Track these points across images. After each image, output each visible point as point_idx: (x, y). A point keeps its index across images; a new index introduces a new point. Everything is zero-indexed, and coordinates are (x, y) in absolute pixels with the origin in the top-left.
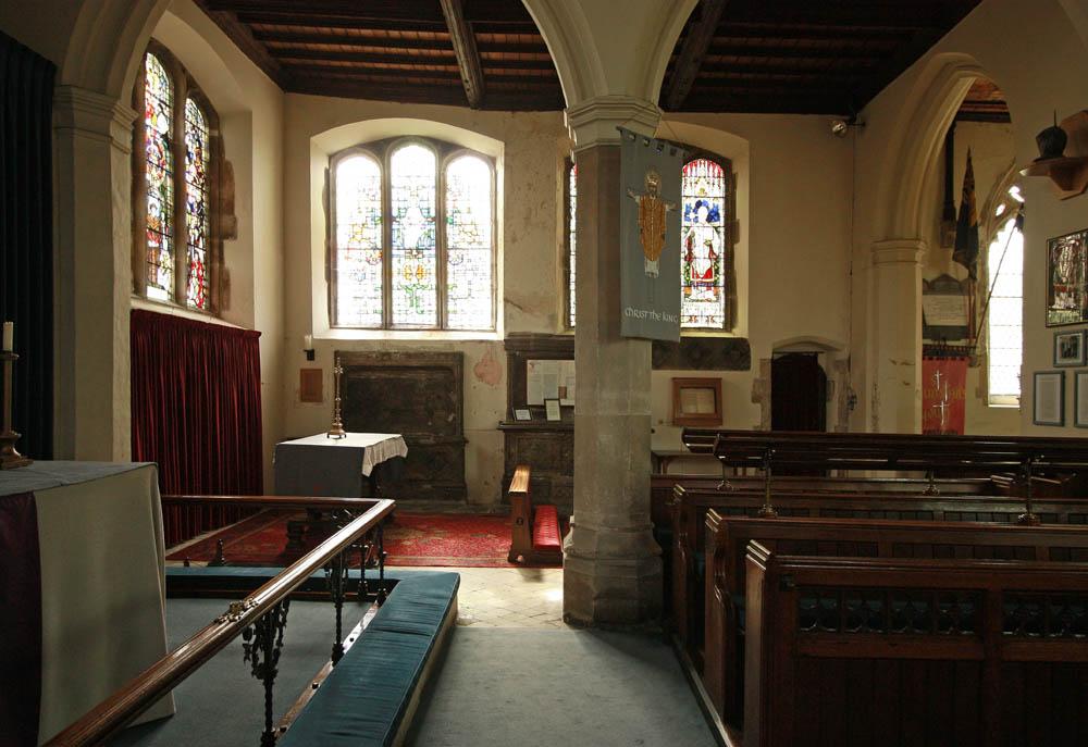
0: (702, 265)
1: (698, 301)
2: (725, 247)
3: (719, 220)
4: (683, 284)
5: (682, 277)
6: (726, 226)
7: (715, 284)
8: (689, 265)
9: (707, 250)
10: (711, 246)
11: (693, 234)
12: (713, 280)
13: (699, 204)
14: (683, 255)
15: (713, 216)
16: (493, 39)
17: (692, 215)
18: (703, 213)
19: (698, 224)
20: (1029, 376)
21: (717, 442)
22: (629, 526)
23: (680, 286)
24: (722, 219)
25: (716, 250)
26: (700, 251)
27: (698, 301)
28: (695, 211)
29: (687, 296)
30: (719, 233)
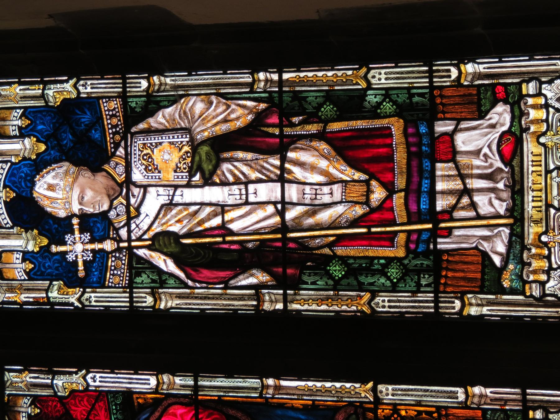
0: (316, 187)
1: (516, 213)
2: (225, 65)
3: (92, 103)
4: (425, 302)
5: (384, 303)
6: (119, 65)
7: (420, 110)
8: (321, 264)
9: (239, 163)
10: (224, 144)
11: (163, 241)
12: (396, 127)
13: (26, 212)
14: (273, 302)
15: (76, 138)
16: (416, 167)
17: (78, 248)
18: (61, 191)
19: (118, 216)
20: (392, 63)
21: (401, 238)
22: (71, 180)
23: (436, 319)
24: (88, 88)
25: (240, 115)
26: (247, 203)
27: (516, 213)
28: (55, 228)
29: (488, 278)
30: (153, 103)
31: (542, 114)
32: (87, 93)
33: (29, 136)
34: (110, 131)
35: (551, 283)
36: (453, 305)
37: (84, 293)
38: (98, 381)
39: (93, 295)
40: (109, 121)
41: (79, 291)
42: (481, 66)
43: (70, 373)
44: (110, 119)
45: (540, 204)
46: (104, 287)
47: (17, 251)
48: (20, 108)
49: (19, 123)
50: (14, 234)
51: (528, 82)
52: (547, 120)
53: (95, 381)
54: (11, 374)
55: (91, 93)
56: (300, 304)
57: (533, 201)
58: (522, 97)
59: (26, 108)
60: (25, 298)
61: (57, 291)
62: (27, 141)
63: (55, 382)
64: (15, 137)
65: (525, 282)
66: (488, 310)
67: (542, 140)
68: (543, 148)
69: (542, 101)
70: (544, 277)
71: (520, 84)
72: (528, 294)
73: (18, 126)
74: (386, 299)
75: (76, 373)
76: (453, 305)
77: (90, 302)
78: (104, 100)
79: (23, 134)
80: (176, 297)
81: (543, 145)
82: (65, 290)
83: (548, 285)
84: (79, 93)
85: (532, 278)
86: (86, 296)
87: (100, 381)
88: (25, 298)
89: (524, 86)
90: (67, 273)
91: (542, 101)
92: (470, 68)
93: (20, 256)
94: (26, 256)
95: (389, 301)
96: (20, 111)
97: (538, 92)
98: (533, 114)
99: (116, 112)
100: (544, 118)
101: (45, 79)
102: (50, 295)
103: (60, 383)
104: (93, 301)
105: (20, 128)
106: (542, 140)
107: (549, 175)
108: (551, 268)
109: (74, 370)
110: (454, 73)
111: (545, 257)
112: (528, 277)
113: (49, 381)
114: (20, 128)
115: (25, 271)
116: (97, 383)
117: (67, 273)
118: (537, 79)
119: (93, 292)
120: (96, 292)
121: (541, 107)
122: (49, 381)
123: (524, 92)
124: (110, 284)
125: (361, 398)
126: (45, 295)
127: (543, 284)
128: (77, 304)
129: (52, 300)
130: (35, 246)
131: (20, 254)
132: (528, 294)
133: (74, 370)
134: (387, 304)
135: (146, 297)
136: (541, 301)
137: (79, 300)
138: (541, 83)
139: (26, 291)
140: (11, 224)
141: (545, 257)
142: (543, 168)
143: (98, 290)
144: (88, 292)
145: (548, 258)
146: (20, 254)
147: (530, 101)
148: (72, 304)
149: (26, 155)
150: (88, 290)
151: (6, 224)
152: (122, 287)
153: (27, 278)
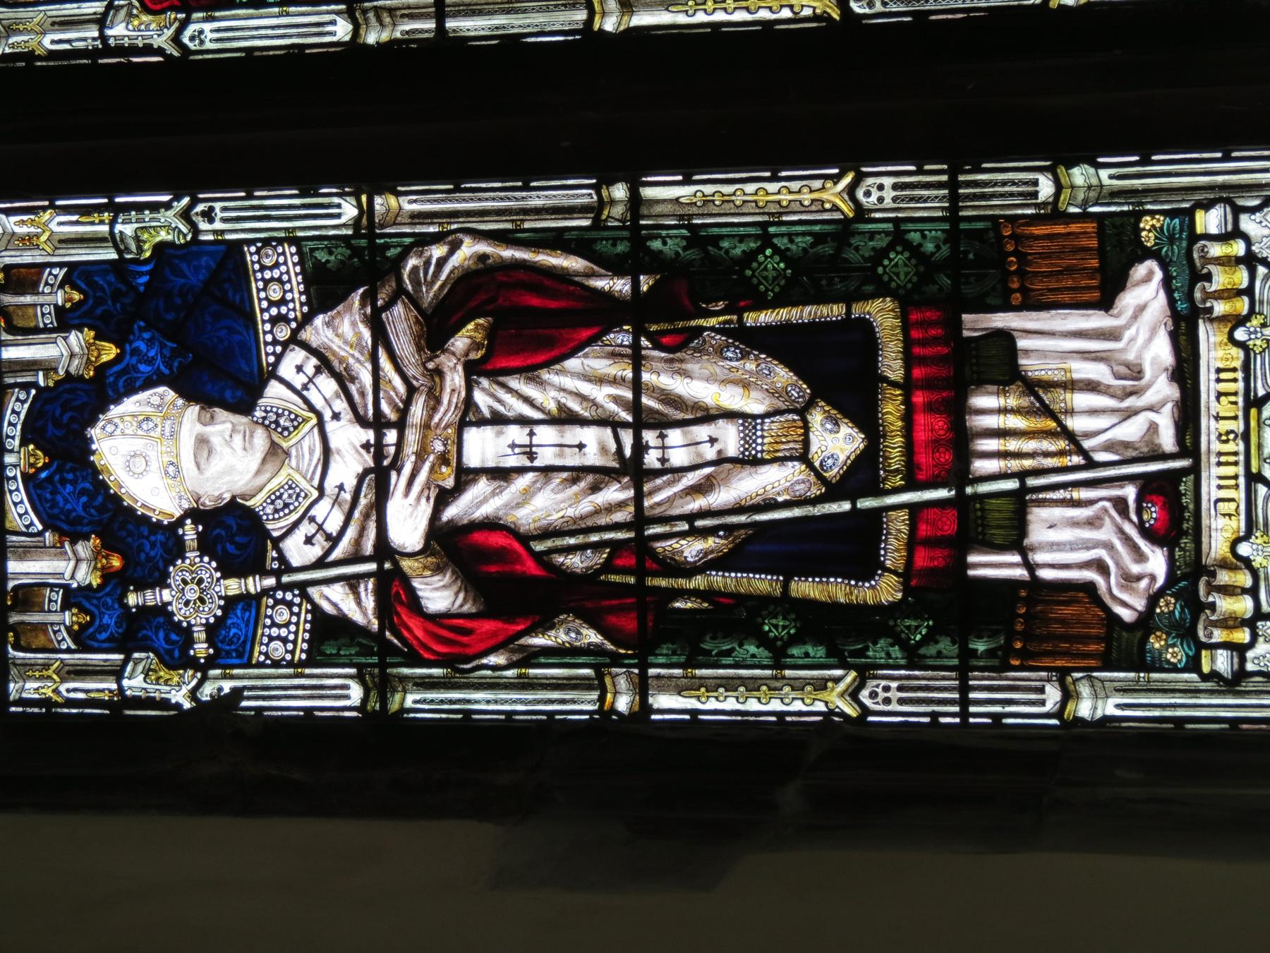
28: (140, 546)
31: (1241, 277)
32: (215, 232)
33: (79, 328)
34: (266, 316)
35: (1261, 648)
36: (1043, 697)
37: (184, 24)
38: (217, 219)
39: (207, 27)
40: (263, 295)
41: (194, 676)
42: (1104, 174)
43: (155, 207)
44: (265, 289)
45: (1230, 471)
46: (249, 665)
47: (52, 586)
48: (60, 265)
49: (60, 298)
50: (45, 547)
51: (1207, 206)
52: (1249, 291)
53: (211, 221)
54: (13, 219)
55: (222, 232)
56: (698, 698)
57: (1219, 464)
58: (1194, 238)
59: (72, 266)
60: (53, 42)
61: (124, 24)
62: (74, 338)
63: (118, 228)
64: (46, 330)
65: (1200, 646)
66: (1118, 706)
67: (1240, 334)
68: (1240, 354)
69: (1239, 248)
70: (1243, 636)
71: (1190, 213)
72: (1206, 669)
73: (56, 306)
74: (894, 685)
75: (167, 206)
76: (1043, 697)
77: (202, 42)
78: (253, 249)
79: (66, 320)
80: (416, 684)
81: (1242, 345)
82: (162, 673)
83: (1250, 654)
84: (195, 230)
85: (1219, 636)
86: (191, 29)
87: (224, 220)
88: (53, 42)
89: (1199, 215)
90: (161, 637)
91: (1239, 248)
92: (1080, 175)
93: (58, 597)
94: (73, 597)
95: (895, 187)
96: (60, 273)
97: (1230, 228)
98: (1221, 279)
99: (282, 274)
100: (1245, 284)
101: (118, 200)
102: (109, 32)
103: (128, 230)
104: (207, 40)
105: (59, 310)
106: (1240, 334)
107: (1253, 411)
108: (1259, 615)
109: (166, 198)
110: (1046, 188)
111: (1244, 591)
112: (1210, 636)
113: (105, 228)
114: (59, 310)
115: (69, 630)
116: (218, 225)
117: (161, 637)
118: (1229, 201)
119: (225, 677)
120: (214, 19)
121: (1238, 261)
122: (105, 228)
123: (1199, 229)
124: (262, 658)
125: (826, 210)
126: (114, 686)
127: (1240, 650)
128: (187, 705)
129: (112, 42)
130: (87, 368)
131: (57, 593)
132: (1206, 669)
133: (166, 198)
134: (895, 695)
135: (333, 23)
136: (1235, 682)
137: (176, 39)
138: (1238, 211)
139: (56, 27)
140: (40, 527)
141: (1244, 591)
142: (1240, 470)
143: (236, 671)
144: (216, 678)
145: (1253, 592)
146: (57, 593)
147: (1216, 250)
148: (160, 51)
149: (72, 370)
150: (196, 15)
151: (27, 527)
152: (290, 664)
153: (73, 647)
